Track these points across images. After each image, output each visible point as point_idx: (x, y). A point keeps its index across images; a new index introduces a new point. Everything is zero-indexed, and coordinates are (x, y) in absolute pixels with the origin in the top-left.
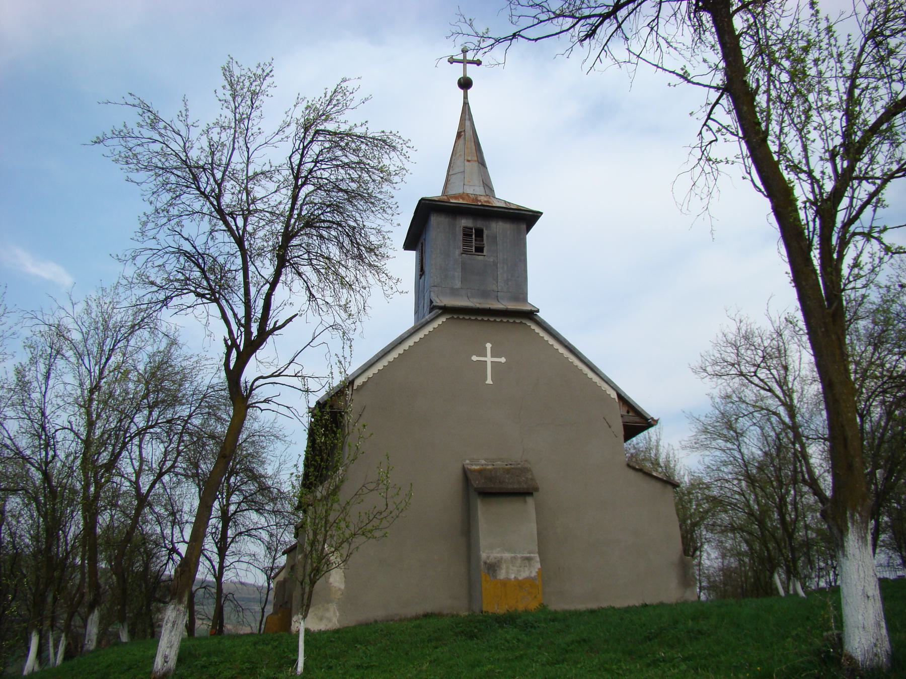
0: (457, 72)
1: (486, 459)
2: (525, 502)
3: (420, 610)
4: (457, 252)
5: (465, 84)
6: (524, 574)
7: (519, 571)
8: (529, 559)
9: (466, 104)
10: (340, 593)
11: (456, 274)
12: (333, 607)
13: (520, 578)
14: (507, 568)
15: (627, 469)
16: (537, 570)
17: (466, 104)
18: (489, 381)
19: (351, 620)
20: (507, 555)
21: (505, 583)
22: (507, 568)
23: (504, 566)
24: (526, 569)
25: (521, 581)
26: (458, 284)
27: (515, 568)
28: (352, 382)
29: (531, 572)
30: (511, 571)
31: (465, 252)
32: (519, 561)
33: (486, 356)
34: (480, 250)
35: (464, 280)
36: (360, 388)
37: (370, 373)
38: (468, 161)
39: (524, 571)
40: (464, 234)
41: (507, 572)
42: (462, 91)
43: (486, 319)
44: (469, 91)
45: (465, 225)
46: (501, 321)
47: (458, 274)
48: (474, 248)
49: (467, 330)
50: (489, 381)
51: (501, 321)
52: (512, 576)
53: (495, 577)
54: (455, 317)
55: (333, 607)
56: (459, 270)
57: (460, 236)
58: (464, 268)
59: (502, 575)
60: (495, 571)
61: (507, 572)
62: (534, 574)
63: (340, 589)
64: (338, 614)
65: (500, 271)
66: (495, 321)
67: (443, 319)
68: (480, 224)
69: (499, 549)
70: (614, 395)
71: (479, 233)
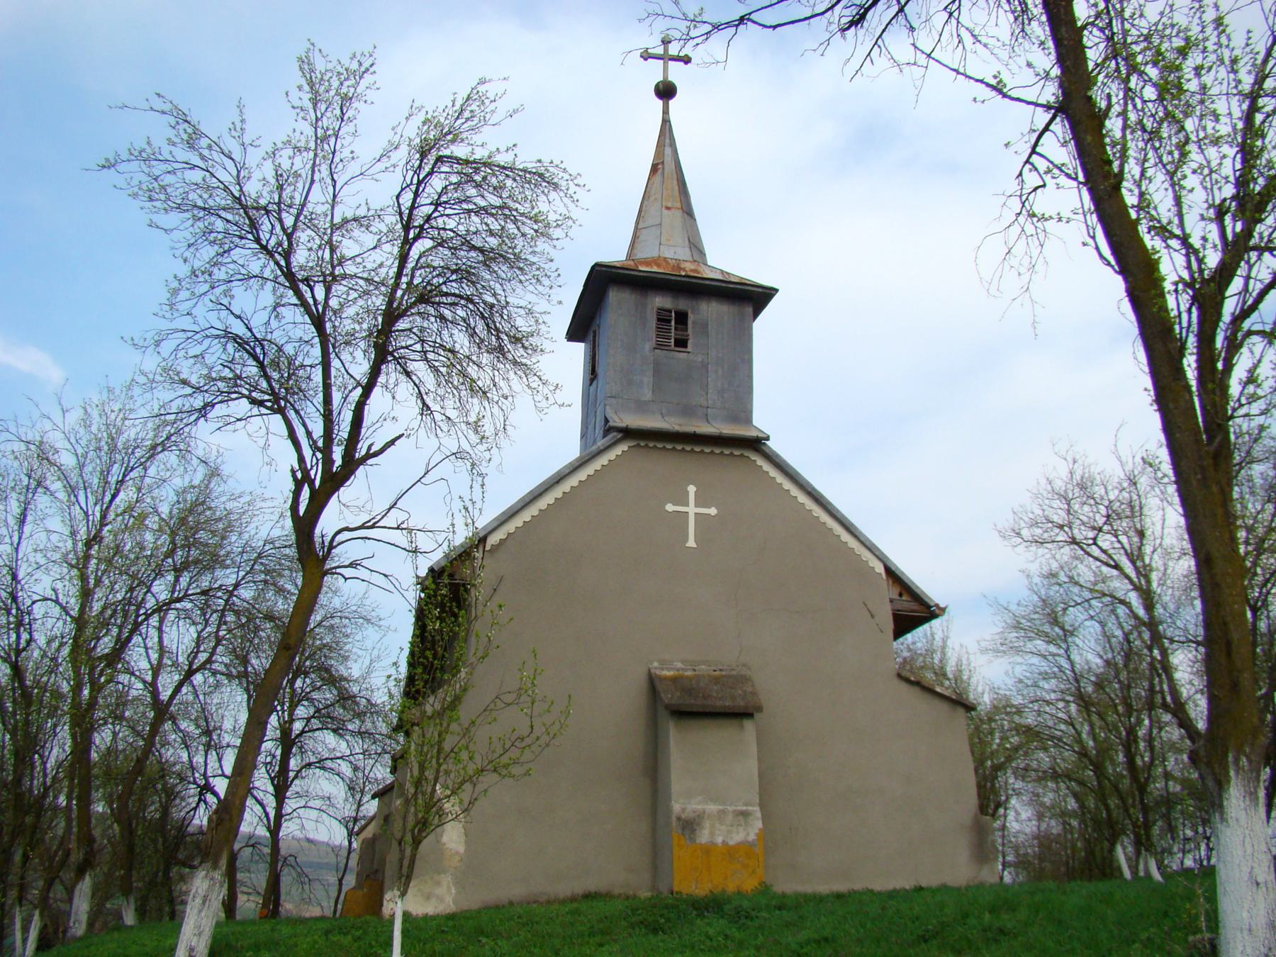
0: (654, 73)
1: (682, 662)
2: (742, 727)
3: (564, 889)
4: (648, 346)
5: (666, 91)
6: (737, 837)
7: (729, 832)
8: (745, 814)
9: (666, 122)
10: (457, 858)
11: (646, 379)
12: (446, 880)
13: (731, 843)
14: (712, 826)
15: (897, 682)
16: (757, 831)
17: (666, 122)
18: (691, 543)
19: (473, 901)
20: (712, 808)
21: (708, 850)
22: (712, 826)
23: (707, 824)
24: (741, 829)
25: (732, 847)
26: (647, 395)
27: (723, 828)
28: (483, 540)
29: (748, 834)
30: (717, 832)
31: (659, 346)
32: (730, 817)
33: (687, 505)
34: (682, 343)
35: (657, 388)
36: (495, 548)
37: (511, 527)
38: (668, 208)
39: (738, 833)
40: (659, 320)
41: (712, 834)
42: (660, 103)
43: (688, 448)
44: (671, 102)
45: (660, 305)
46: (712, 452)
47: (648, 379)
48: (673, 341)
49: (661, 464)
50: (691, 543)
51: (712, 452)
52: (719, 840)
53: (693, 840)
54: (642, 444)
55: (446, 880)
56: (650, 373)
57: (652, 322)
58: (657, 371)
59: (704, 837)
60: (693, 831)
61: (712, 834)
62: (752, 837)
63: (457, 853)
64: (453, 891)
65: (712, 376)
66: (702, 452)
67: (623, 447)
68: (683, 304)
69: (700, 798)
70: (880, 569)
71: (682, 318)
